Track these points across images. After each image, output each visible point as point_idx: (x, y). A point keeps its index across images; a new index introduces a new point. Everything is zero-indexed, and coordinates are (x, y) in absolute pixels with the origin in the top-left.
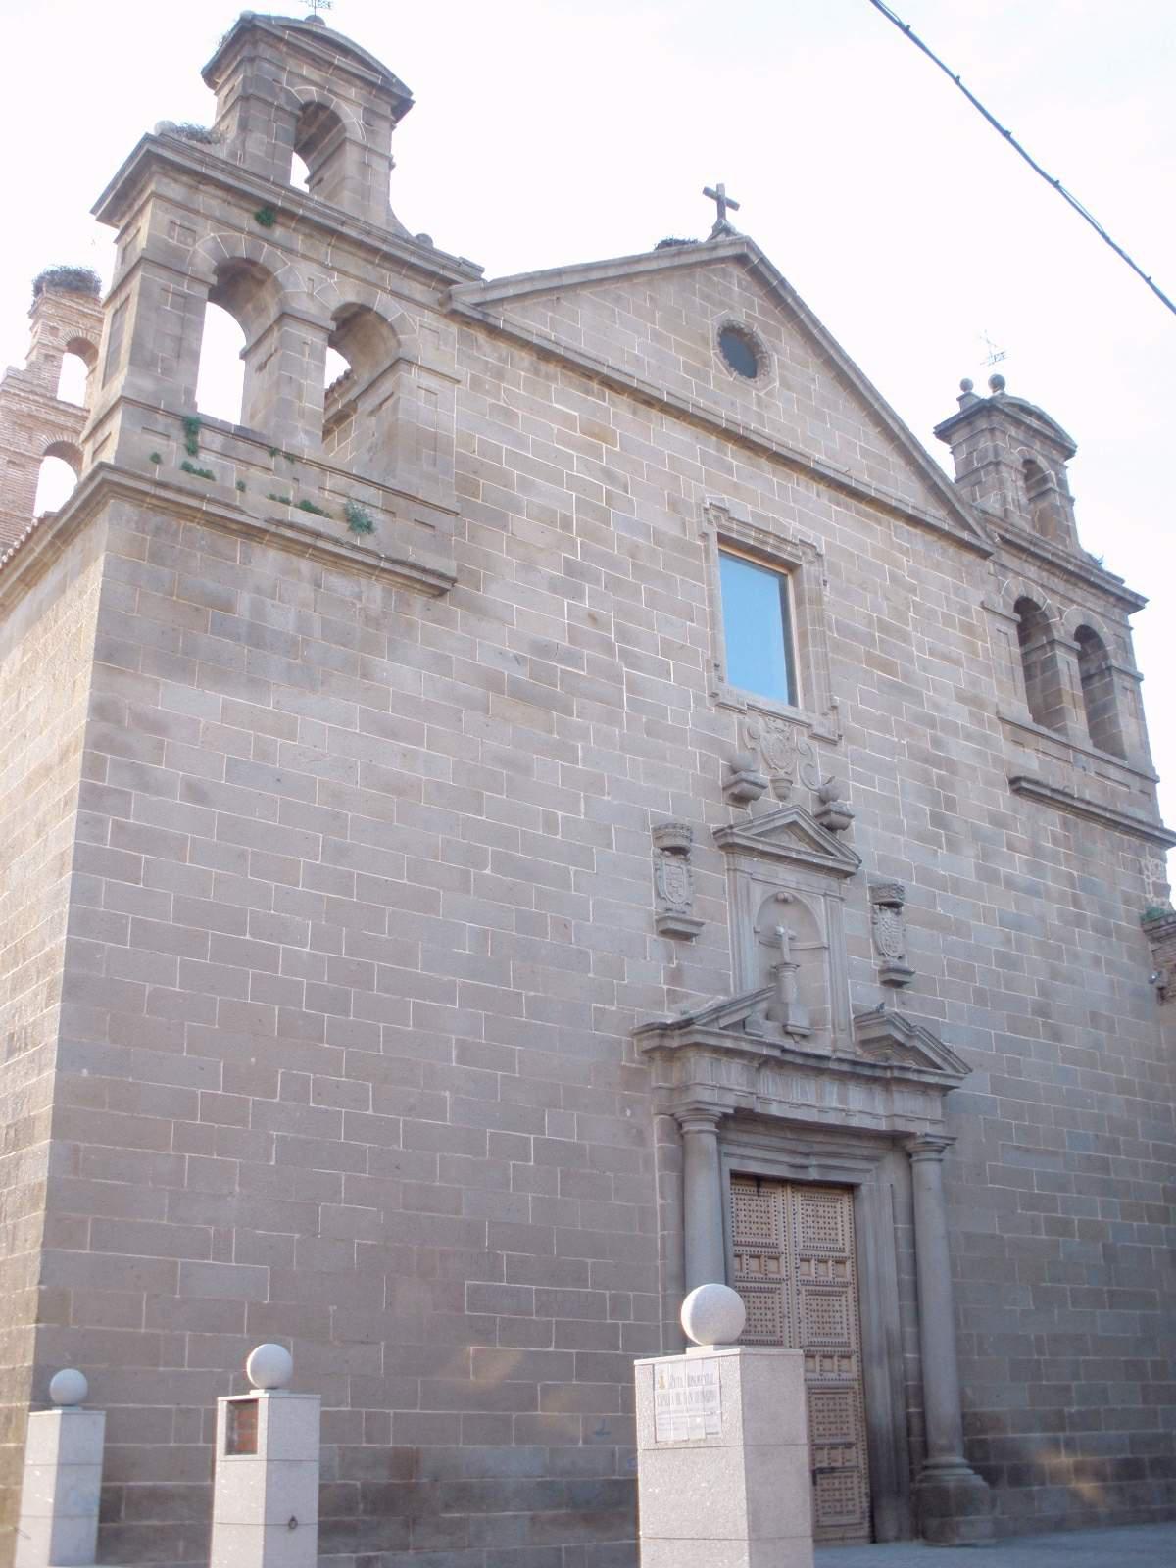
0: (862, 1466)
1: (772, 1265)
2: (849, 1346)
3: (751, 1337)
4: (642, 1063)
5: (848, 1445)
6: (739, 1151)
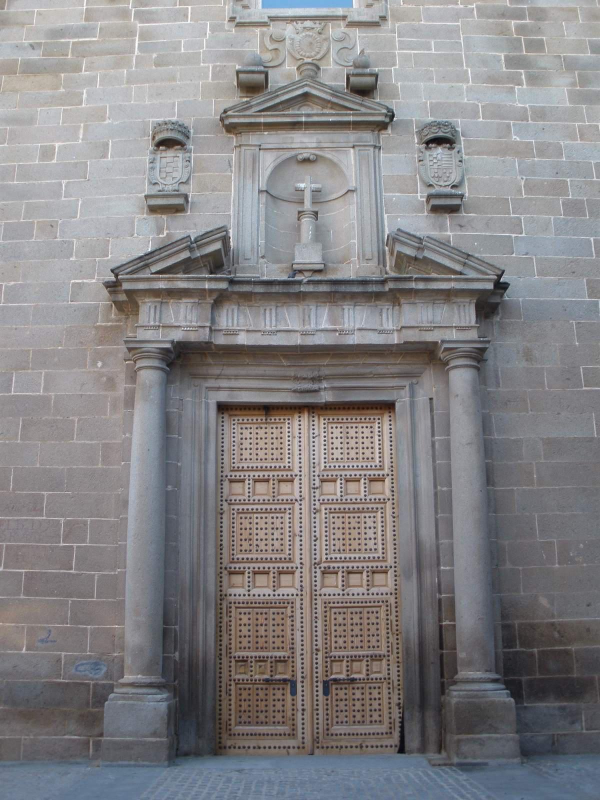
1: (285, 488)
2: (386, 561)
3: (254, 556)
4: (117, 321)
5: (378, 658)
6: (224, 383)
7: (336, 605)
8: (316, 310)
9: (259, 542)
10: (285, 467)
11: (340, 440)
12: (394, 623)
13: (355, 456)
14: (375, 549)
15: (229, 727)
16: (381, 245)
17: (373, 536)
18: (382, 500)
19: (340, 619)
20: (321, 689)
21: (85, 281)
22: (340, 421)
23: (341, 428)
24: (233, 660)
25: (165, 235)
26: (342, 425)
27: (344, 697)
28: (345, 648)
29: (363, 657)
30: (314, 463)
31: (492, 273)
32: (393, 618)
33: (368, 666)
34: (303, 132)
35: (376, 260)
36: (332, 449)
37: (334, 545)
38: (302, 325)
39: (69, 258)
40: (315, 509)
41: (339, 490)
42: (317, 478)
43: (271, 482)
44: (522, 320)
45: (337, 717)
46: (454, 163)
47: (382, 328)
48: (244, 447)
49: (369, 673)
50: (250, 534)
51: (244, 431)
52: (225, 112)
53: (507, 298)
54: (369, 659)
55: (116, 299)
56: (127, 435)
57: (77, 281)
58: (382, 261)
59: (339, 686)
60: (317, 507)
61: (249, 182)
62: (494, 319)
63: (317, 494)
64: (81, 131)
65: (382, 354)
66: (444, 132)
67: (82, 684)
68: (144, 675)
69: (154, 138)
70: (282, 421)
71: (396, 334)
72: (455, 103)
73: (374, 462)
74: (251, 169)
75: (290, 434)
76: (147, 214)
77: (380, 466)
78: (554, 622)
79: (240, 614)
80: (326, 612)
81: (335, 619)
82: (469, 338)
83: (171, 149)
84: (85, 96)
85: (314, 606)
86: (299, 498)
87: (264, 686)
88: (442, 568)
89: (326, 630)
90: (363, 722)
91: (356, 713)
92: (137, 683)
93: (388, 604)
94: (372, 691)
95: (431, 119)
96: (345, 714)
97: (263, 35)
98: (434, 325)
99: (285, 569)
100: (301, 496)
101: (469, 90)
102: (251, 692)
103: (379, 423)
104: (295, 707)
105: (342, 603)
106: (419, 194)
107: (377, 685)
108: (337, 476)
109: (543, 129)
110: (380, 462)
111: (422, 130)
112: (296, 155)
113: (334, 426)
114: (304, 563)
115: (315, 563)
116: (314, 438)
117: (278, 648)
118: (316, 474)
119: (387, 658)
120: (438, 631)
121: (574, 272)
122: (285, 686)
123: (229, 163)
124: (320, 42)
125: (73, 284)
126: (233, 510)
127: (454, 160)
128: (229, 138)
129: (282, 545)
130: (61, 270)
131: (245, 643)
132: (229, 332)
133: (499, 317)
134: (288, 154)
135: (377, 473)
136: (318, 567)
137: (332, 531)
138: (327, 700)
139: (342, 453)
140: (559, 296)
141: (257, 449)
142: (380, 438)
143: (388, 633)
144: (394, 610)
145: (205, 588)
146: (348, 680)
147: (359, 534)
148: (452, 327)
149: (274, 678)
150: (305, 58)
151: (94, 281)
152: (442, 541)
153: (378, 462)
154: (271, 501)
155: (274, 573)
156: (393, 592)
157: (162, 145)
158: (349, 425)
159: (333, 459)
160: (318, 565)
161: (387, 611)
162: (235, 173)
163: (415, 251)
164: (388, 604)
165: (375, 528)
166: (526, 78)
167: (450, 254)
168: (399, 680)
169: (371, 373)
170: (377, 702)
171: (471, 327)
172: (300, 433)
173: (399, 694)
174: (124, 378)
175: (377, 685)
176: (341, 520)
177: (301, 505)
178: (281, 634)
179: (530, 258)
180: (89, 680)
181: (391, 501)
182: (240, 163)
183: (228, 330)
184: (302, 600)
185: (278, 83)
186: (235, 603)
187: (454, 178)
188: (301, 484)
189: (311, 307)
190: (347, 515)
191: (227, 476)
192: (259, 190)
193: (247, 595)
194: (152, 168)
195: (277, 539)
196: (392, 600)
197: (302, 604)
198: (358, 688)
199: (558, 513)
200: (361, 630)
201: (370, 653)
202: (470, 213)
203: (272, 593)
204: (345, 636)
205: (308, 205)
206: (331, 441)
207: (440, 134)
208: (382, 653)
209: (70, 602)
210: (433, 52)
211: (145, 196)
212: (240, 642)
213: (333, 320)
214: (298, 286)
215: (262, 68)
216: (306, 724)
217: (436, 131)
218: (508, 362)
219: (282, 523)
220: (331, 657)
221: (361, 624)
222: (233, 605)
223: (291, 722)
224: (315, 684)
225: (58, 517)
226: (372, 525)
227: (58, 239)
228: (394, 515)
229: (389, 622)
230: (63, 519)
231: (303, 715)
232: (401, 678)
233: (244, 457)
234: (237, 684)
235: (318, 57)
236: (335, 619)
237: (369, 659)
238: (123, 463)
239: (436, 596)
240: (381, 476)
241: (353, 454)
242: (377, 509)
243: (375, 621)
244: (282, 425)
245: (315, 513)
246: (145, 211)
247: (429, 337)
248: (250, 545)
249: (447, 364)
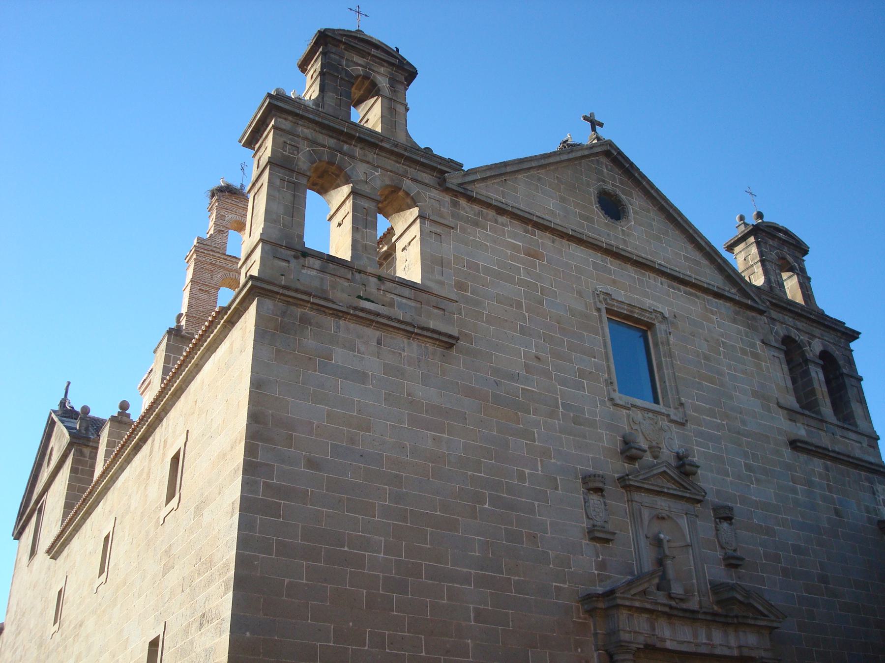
25: (601, 559)
76: (589, 541)
128: (622, 492)
157: (592, 491)
192: (63, 404)
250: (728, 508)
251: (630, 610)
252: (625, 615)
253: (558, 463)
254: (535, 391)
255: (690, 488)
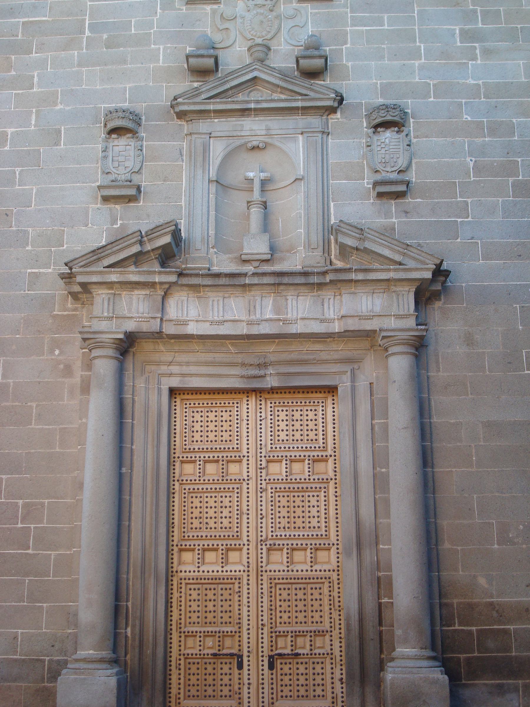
0: (337, 652)
1: (233, 468)
5: (321, 633)
6: (175, 369)
7: (281, 581)
8: (261, 300)
9: (208, 520)
10: (233, 448)
11: (285, 423)
12: (337, 599)
13: (299, 438)
14: (319, 527)
15: (178, 701)
16: (326, 234)
17: (316, 514)
18: (325, 480)
19: (285, 594)
20: (266, 663)
21: (41, 270)
22: (286, 404)
23: (287, 411)
24: (182, 635)
25: (119, 225)
26: (287, 408)
27: (288, 672)
28: (289, 623)
29: (307, 632)
30: (261, 445)
31: (430, 262)
32: (336, 594)
33: (311, 641)
34: (253, 119)
35: (321, 248)
36: (278, 431)
37: (279, 523)
38: (248, 315)
39: (25, 247)
40: (261, 488)
41: (284, 470)
42: (263, 458)
43: (221, 463)
44: (465, 305)
45: (282, 691)
46: (402, 147)
47: (323, 317)
48: (195, 429)
49: (313, 648)
50: (201, 513)
51: (195, 414)
52: (175, 99)
53: (450, 284)
54: (312, 634)
55: (72, 290)
56: (84, 420)
57: (34, 271)
58: (327, 250)
59: (283, 661)
60: (264, 486)
61: (200, 172)
62: (436, 305)
63: (264, 474)
64: (34, 117)
65: (325, 341)
66: (392, 116)
67: (38, 660)
68: (95, 651)
69: (105, 125)
70: (231, 404)
71: (337, 323)
72: (405, 83)
73: (318, 443)
74: (201, 159)
75: (238, 417)
76: (101, 204)
77: (324, 447)
78: (493, 602)
79: (190, 589)
80: (271, 588)
81: (280, 595)
82: (408, 326)
83: (122, 137)
84: (36, 79)
85: (260, 582)
86: (246, 478)
87: (212, 661)
88: (381, 546)
89: (271, 605)
90: (307, 696)
91: (300, 688)
92: (89, 658)
93: (331, 580)
94: (316, 665)
95: (381, 101)
96: (289, 688)
97: (214, 12)
98: (374, 314)
99: (233, 546)
100: (248, 476)
101: (422, 68)
102: (199, 666)
103: (323, 406)
104: (241, 681)
105: (287, 579)
106: (366, 181)
107: (320, 660)
108: (282, 456)
109: (496, 107)
110: (323, 443)
111: (371, 113)
112: (246, 143)
113: (280, 409)
114: (251, 540)
115: (261, 540)
116: (261, 420)
117: (226, 623)
118: (263, 455)
119: (330, 634)
120: (377, 609)
121: (520, 256)
122: (232, 660)
123: (181, 152)
124: (271, 21)
125: (29, 273)
126: (185, 489)
127: (401, 144)
128: (180, 125)
129: (230, 523)
130: (18, 259)
131: (194, 619)
132: (179, 323)
133: (441, 302)
134: (238, 142)
135: (320, 454)
136: (264, 544)
137: (278, 509)
138: (272, 674)
139: (287, 435)
140: (504, 281)
141: (208, 431)
142: (324, 420)
143: (331, 609)
144: (336, 586)
145: (156, 566)
146: (292, 654)
147: (303, 512)
148: (391, 315)
149: (221, 652)
150: (256, 38)
151: (50, 270)
152: (381, 520)
153: (321, 443)
154: (220, 481)
155: (222, 550)
156: (336, 568)
158: (295, 409)
159: (279, 441)
160: (264, 542)
161: (330, 587)
162: (186, 163)
163: (356, 241)
164: (331, 580)
165: (318, 506)
166: (480, 53)
167: (389, 244)
168: (341, 656)
169: (314, 359)
170: (321, 677)
171: (409, 315)
172: (248, 416)
173: (342, 670)
174: (80, 365)
175: (320, 660)
176: (286, 499)
177: (248, 484)
178: (228, 609)
179: (476, 242)
180: (44, 656)
181: (333, 481)
182: (190, 152)
183: (178, 321)
184: (248, 576)
185: (228, 65)
186: (185, 579)
187: (402, 163)
188: (248, 464)
189: (256, 298)
190: (292, 494)
191: (179, 457)
193: (196, 571)
194: (105, 157)
195: (226, 517)
196: (335, 576)
197: (248, 580)
198: (302, 663)
199: (497, 494)
200: (305, 605)
201: (313, 629)
202: (417, 199)
203: (220, 569)
204: (289, 612)
205: (256, 195)
206: (277, 423)
207: (389, 118)
208: (324, 629)
209: (27, 581)
210: (386, 27)
211: (98, 187)
212: (190, 618)
213: (277, 310)
214: (244, 278)
215: (212, 52)
216: (252, 698)
217: (384, 115)
218: (449, 347)
219: (230, 502)
220: (276, 632)
221: (305, 600)
222: (183, 581)
223: (237, 696)
224: (261, 659)
225: (16, 499)
226: (316, 504)
227: (14, 229)
228: (336, 494)
229: (332, 598)
230: (21, 501)
231: (249, 688)
232: (343, 654)
233: (195, 439)
234: (186, 658)
235: (269, 37)
236: (280, 595)
237: (312, 634)
238: (79, 447)
239: (375, 573)
240: (324, 457)
241: (298, 436)
242: (320, 488)
243: (318, 597)
244: (231, 409)
245: (261, 493)
246: (99, 201)
247: (368, 326)
248: (201, 523)
249: (386, 350)
250: (384, 107)
251: (112, 288)
252: (104, 296)
253: (67, 108)
254: (47, 21)
255: (308, 92)
